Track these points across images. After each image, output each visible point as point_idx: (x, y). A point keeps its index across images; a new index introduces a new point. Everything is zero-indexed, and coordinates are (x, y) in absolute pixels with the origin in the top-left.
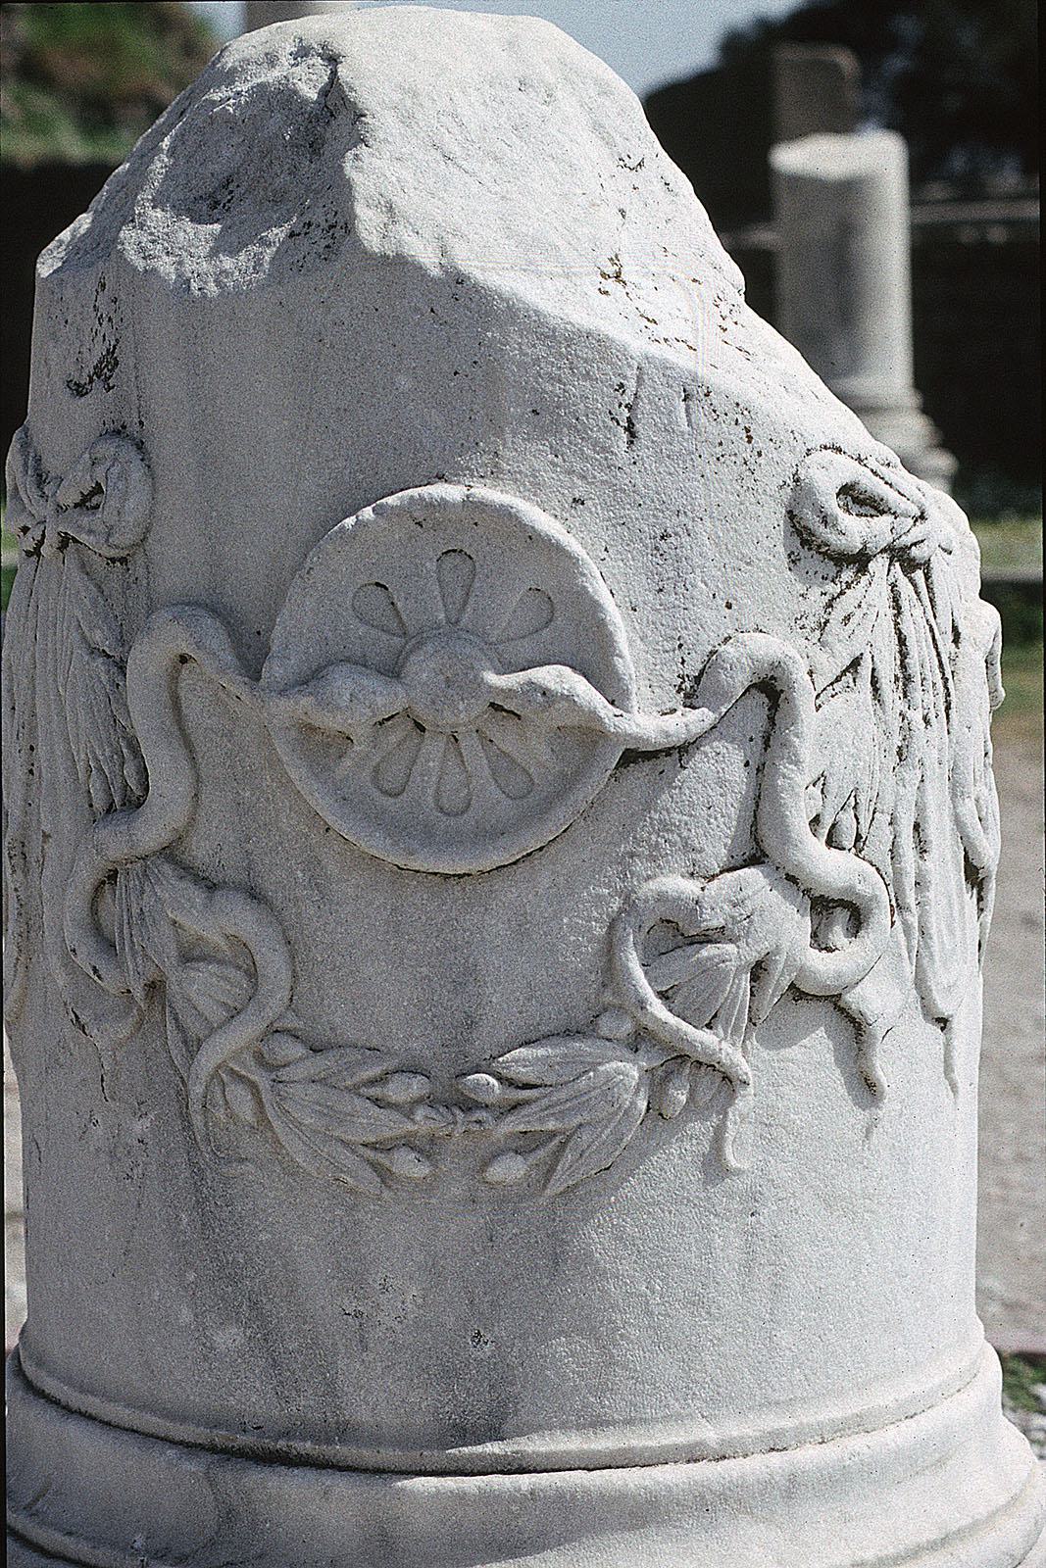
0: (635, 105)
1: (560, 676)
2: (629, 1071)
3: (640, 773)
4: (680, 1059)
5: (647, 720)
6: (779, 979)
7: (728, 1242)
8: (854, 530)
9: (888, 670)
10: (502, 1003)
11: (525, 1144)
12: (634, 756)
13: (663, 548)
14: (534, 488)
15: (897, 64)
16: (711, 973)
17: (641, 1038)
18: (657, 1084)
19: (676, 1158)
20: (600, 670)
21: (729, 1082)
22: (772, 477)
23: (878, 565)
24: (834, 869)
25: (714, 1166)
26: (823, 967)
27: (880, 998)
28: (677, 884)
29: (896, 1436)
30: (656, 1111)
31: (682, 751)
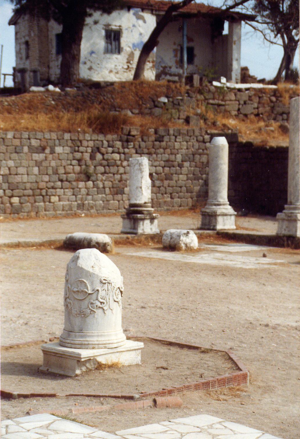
0: (154, 335)
1: (104, 237)
2: (89, 311)
3: (90, 295)
4: (92, 310)
5: (90, 292)
6: (98, 306)
7: (95, 321)
8: (104, 282)
9: (107, 289)
10: (83, 307)
11: (84, 314)
12: (89, 294)
13: (92, 283)
14: (85, 279)
15: (283, 30)
16: (94, 306)
17: (90, 309)
18: (91, 311)
19: (91, 316)
20: (87, 289)
21: (95, 312)
22: (99, 279)
23: (107, 284)
24: (102, 301)
25: (94, 317)
26: (101, 306)
27: (105, 308)
28: (92, 301)
29: (106, 334)
30: (91, 313)
31: (92, 294)
